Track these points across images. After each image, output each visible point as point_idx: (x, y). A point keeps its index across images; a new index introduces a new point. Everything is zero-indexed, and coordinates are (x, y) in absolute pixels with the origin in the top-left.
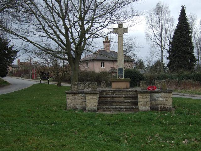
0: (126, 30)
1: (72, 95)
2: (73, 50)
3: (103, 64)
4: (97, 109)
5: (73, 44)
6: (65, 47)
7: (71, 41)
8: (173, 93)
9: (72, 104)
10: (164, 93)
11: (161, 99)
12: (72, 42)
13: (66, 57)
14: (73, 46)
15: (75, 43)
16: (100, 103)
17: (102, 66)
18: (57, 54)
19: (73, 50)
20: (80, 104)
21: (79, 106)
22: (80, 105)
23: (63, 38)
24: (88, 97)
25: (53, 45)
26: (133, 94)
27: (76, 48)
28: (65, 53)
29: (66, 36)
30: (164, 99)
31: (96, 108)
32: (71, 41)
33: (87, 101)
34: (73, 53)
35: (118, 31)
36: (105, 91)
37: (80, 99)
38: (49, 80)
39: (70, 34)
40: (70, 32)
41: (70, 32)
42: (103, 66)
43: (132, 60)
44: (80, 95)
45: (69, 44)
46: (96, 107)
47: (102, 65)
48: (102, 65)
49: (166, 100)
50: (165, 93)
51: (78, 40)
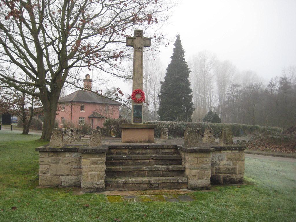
0: (147, 41)
1: (52, 154)
2: (48, 83)
3: (83, 107)
4: (104, 185)
5: (49, 73)
6: (35, 76)
7: (46, 68)
8: (245, 151)
9: (51, 172)
10: (230, 152)
11: (224, 162)
12: (48, 70)
13: (38, 90)
14: (48, 76)
15: (52, 72)
16: (109, 173)
17: (81, 110)
18: (25, 86)
19: (48, 83)
20: (67, 172)
21: (64, 177)
22: (68, 175)
23: (35, 65)
24: (86, 162)
25: (20, 75)
26: (169, 153)
27: (54, 80)
28: (37, 86)
29: (39, 61)
30: (231, 162)
31: (102, 183)
32: (46, 68)
33: (84, 168)
34: (48, 86)
35: (135, 41)
36: (116, 147)
37: (67, 164)
38: (12, 126)
39: (45, 59)
40: (45, 56)
41: (44, 55)
42: (83, 110)
43: (117, 104)
44: (67, 155)
45: (41, 72)
46: (103, 181)
47: (82, 108)
48: (82, 108)
49: (233, 164)
50: (233, 151)
51: (55, 69)
